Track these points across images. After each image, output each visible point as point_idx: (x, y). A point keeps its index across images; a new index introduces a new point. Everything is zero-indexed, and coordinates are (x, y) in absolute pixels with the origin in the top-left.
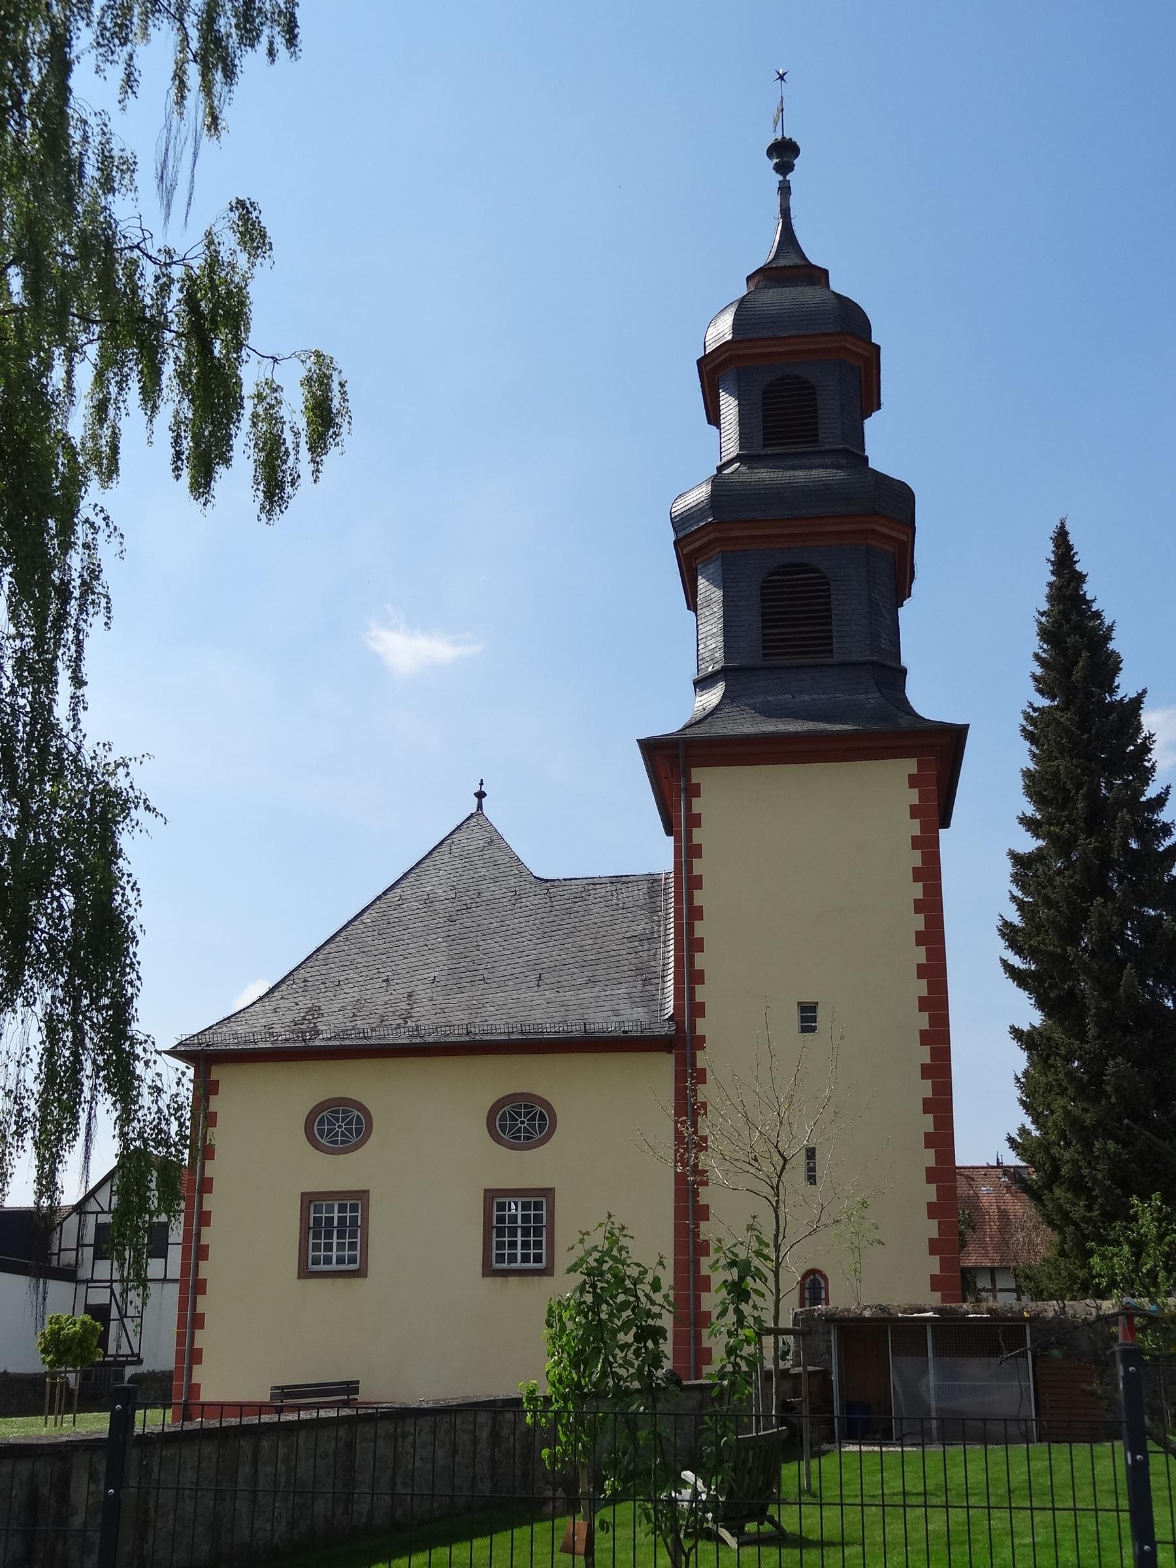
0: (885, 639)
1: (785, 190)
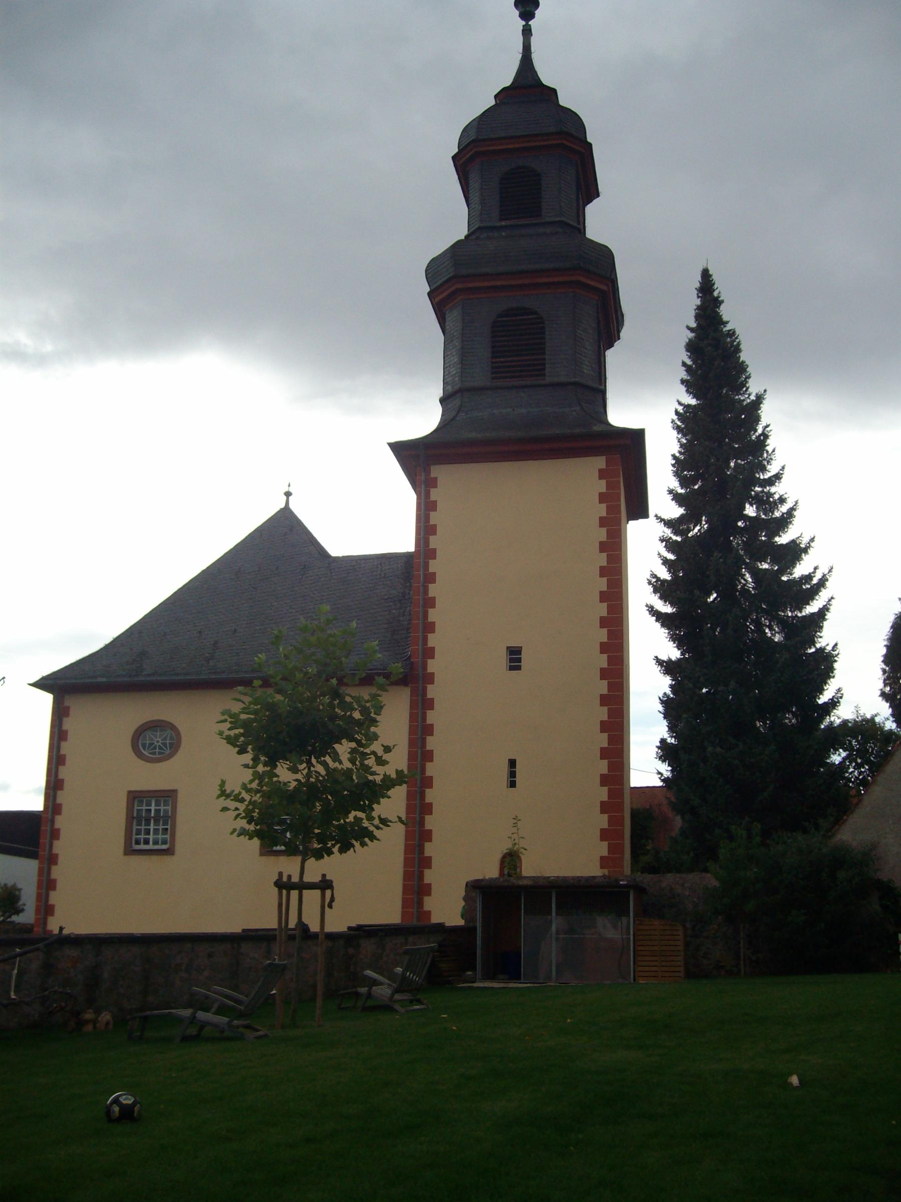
0: (588, 366)
1: (527, 32)
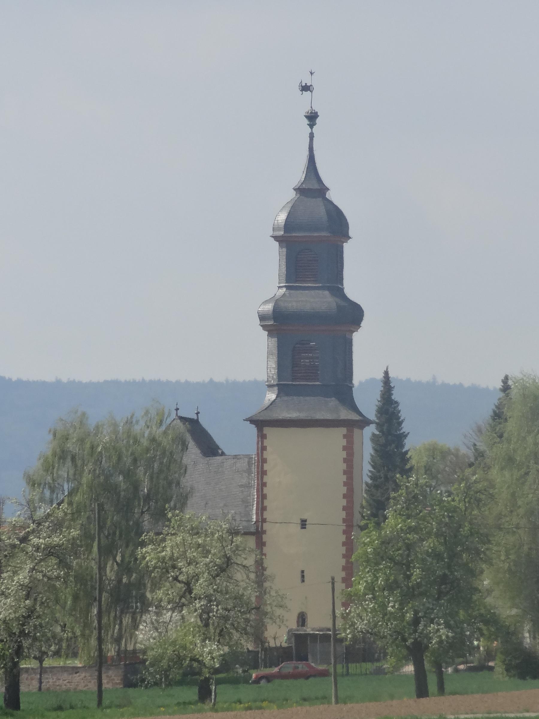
1: (312, 136)
